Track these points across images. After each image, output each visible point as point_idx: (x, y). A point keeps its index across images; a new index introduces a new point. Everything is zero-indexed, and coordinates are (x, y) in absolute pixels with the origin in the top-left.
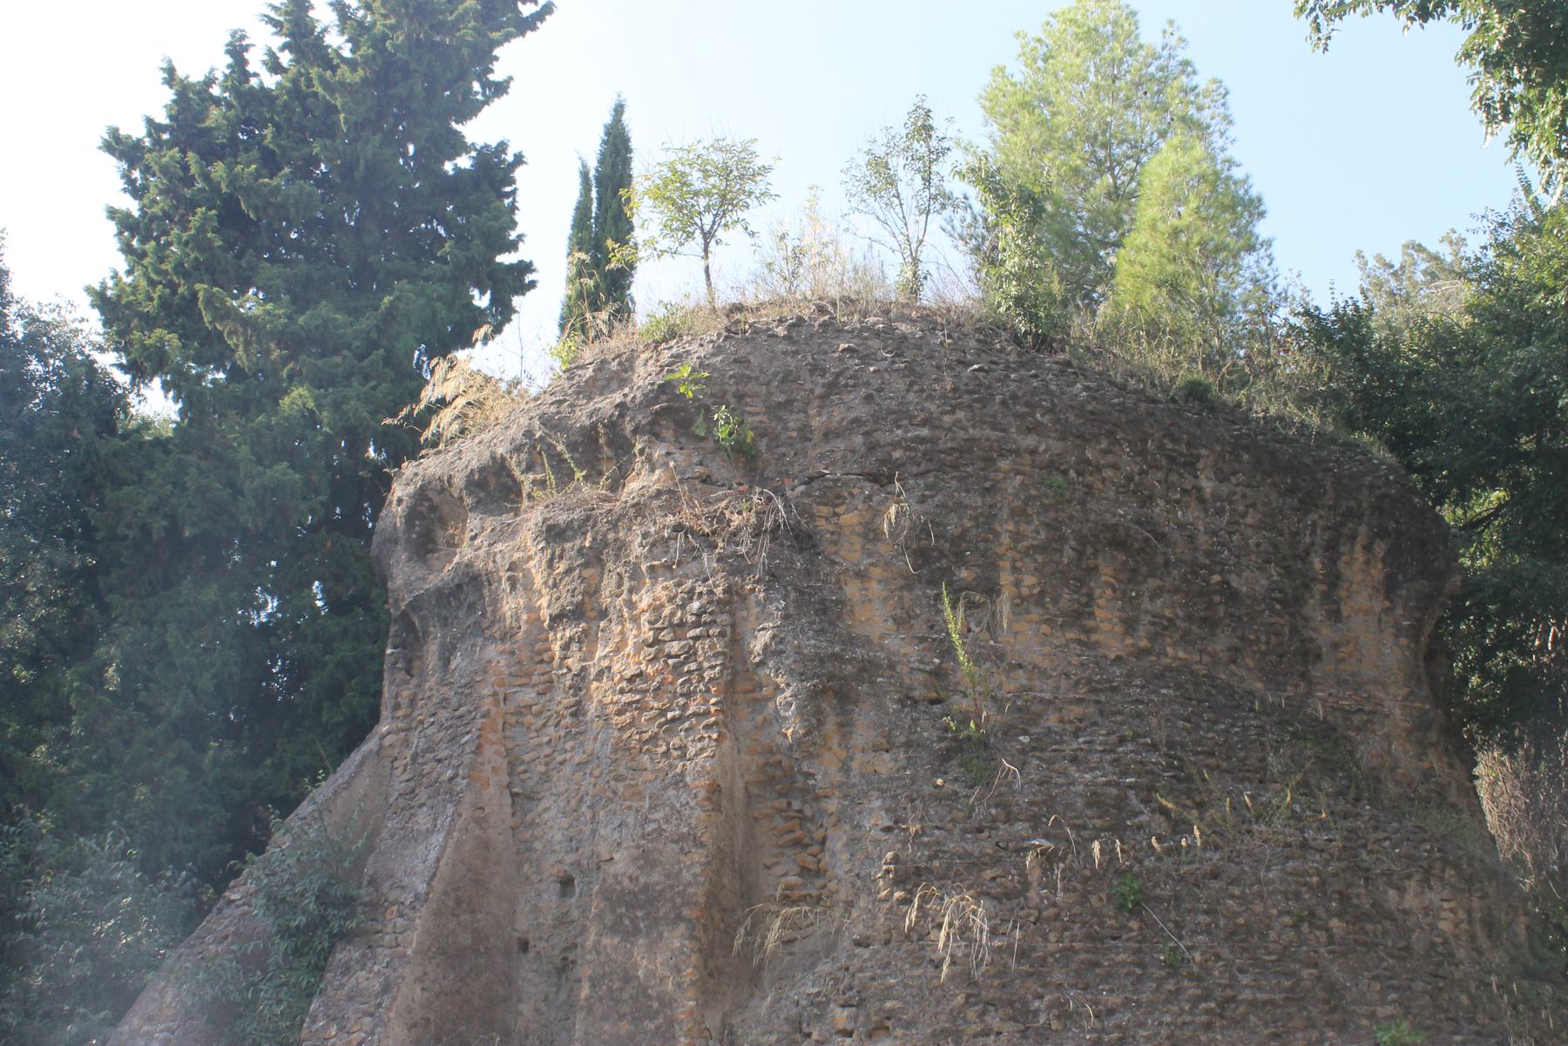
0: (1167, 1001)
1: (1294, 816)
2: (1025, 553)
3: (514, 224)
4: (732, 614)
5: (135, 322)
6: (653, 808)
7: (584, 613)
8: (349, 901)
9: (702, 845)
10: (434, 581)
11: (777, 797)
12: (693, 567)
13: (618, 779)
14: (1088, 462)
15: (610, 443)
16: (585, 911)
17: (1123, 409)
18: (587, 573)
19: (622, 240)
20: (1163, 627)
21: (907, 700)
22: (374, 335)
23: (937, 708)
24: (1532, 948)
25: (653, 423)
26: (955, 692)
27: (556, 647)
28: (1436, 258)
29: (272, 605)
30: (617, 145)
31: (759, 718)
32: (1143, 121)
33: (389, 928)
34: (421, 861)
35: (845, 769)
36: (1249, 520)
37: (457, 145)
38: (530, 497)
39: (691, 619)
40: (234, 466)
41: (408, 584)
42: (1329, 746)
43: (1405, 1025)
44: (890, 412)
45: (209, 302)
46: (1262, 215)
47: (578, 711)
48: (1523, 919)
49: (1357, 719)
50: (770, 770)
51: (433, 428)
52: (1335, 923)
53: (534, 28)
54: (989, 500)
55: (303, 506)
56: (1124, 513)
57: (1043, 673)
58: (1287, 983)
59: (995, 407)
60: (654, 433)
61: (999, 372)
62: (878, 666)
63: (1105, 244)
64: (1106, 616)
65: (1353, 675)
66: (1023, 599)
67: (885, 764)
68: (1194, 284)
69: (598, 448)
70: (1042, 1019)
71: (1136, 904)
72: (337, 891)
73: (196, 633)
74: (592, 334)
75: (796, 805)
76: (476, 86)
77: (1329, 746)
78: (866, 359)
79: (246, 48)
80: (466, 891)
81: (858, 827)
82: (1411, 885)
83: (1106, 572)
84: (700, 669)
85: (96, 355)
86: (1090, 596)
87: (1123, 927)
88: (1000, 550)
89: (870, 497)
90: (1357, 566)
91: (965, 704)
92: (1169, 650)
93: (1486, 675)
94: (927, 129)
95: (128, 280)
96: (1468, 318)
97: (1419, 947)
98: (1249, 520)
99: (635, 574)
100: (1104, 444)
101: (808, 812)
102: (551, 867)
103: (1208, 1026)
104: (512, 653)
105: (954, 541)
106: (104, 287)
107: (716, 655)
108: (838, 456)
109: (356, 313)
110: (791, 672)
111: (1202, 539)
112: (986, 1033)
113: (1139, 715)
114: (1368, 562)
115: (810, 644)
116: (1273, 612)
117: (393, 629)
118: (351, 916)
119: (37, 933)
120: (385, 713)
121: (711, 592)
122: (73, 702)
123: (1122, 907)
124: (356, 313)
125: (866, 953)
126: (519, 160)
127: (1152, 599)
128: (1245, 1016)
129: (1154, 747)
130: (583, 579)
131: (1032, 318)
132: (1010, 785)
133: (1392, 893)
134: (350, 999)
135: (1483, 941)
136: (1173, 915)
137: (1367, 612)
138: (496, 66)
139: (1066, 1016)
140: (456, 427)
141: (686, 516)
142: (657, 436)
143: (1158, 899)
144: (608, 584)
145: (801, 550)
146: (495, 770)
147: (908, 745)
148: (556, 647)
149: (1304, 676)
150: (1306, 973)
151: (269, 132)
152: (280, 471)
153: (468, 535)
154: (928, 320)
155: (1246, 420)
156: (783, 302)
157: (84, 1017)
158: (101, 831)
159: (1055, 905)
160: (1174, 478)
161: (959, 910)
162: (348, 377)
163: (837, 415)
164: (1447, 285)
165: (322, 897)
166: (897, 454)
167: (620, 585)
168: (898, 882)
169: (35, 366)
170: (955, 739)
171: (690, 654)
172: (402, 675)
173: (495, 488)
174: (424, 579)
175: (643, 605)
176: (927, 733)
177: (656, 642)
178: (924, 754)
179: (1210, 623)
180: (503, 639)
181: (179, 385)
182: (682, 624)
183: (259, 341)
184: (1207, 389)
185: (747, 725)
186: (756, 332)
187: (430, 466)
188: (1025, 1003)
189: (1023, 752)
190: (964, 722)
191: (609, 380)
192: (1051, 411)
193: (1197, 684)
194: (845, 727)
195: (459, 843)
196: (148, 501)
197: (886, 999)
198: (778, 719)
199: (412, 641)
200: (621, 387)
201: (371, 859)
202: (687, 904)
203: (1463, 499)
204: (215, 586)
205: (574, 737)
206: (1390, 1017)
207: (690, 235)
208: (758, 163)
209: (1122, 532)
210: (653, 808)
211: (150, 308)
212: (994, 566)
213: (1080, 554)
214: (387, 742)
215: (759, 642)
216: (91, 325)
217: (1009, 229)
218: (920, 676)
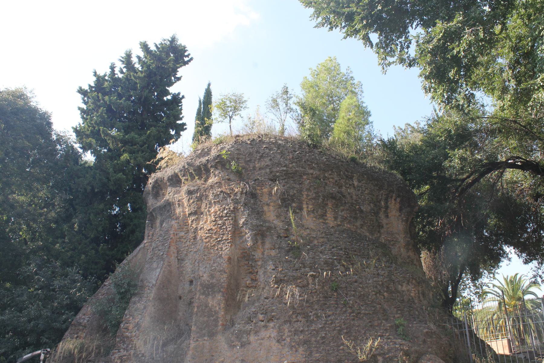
0: (343, 313)
1: (376, 267)
2: (310, 200)
3: (181, 113)
4: (235, 214)
5: (84, 136)
6: (214, 263)
7: (197, 213)
8: (135, 286)
9: (226, 273)
10: (159, 204)
11: (245, 260)
12: (225, 202)
13: (205, 256)
14: (326, 177)
15: (205, 170)
16: (196, 289)
17: (335, 164)
18: (198, 203)
19: (209, 118)
20: (344, 219)
21: (279, 237)
22: (145, 141)
23: (287, 239)
24: (434, 301)
25: (215, 165)
26: (291, 235)
27: (190, 222)
28: (413, 127)
29: (117, 209)
30: (208, 94)
31: (241, 241)
32: (341, 91)
33: (146, 292)
34: (153, 276)
35: (263, 254)
36: (366, 192)
37: (167, 93)
38: (184, 183)
39: (224, 215)
40: (108, 173)
41: (152, 205)
42: (384, 249)
43: (402, 319)
44: (276, 163)
45: (103, 132)
46: (370, 115)
47: (195, 238)
48: (431, 293)
49: (392, 243)
50: (244, 254)
51: (159, 165)
52: (385, 294)
53: (188, 64)
54: (301, 186)
55: (126, 184)
56: (335, 190)
57: (314, 230)
58: (373, 309)
59: (303, 163)
60: (216, 167)
61: (304, 154)
62: (272, 228)
63: (331, 122)
64: (330, 216)
65: (391, 232)
66: (309, 211)
67: (273, 253)
68: (353, 132)
69: (202, 171)
70: (312, 318)
71: (336, 289)
72: (133, 283)
73: (98, 216)
74: (201, 142)
75: (250, 263)
76: (173, 78)
77: (384, 249)
78: (270, 150)
79: (115, 67)
80: (166, 283)
81: (266, 269)
82: (405, 284)
83: (330, 205)
84: (226, 228)
85: (74, 144)
86: (326, 211)
87: (333, 295)
88: (303, 199)
89: (270, 185)
90: (393, 204)
91: (294, 238)
92: (346, 225)
93: (423, 232)
94: (287, 92)
95: (83, 125)
96: (421, 143)
97: (406, 300)
98: (366, 192)
99: (210, 203)
100: (330, 173)
101: (253, 265)
102: (187, 278)
103: (353, 320)
104: (178, 223)
105: (292, 196)
106: (77, 127)
107: (231, 224)
108: (263, 174)
109: (140, 135)
110: (250, 229)
111: (354, 197)
112: (297, 321)
113: (338, 241)
114: (395, 203)
115: (255, 222)
116: (372, 216)
117: (148, 216)
118: (136, 289)
119: (56, 292)
120: (146, 237)
121: (229, 208)
122: (66, 234)
123: (332, 290)
124: (140, 135)
125: (268, 301)
126: (183, 97)
127: (341, 212)
128: (362, 317)
129: (341, 249)
130: (197, 204)
131: (313, 140)
132: (305, 258)
133: (400, 286)
134: (136, 310)
135: (422, 298)
136: (345, 292)
137: (395, 216)
138: (178, 73)
139: (318, 317)
140: (165, 165)
141: (223, 189)
142: (217, 168)
143: (342, 288)
144: (203, 206)
145: (253, 198)
146: (173, 253)
147: (279, 248)
148: (190, 222)
149: (379, 232)
150: (378, 306)
151: (120, 89)
152: (120, 175)
153: (168, 192)
154: (286, 140)
155: (366, 167)
156: (249, 135)
157: (67, 314)
158: (72, 266)
159: (315, 289)
160: (347, 181)
161: (291, 291)
162: (138, 151)
163: (263, 164)
164: (416, 134)
165: (129, 284)
166: (278, 174)
167: (206, 206)
168: (276, 283)
169: (58, 147)
170: (291, 247)
171: (224, 224)
172: (150, 228)
173: (175, 180)
174: (156, 204)
175: (212, 211)
176: (284, 245)
177: (215, 221)
178: (283, 250)
179: (356, 218)
180: (176, 219)
181: (95, 153)
182: (222, 216)
183: (116, 142)
184: (356, 159)
185: (238, 242)
186: (242, 142)
187: (158, 175)
188: (308, 314)
189: (308, 250)
190: (293, 242)
191: (205, 154)
192: (317, 164)
193: (352, 234)
194: (263, 243)
195: (164, 271)
196: (86, 182)
197: (273, 312)
198: (246, 241)
199: (153, 220)
200: (208, 156)
201: (141, 275)
202: (222, 288)
203: (419, 188)
204: (103, 204)
205: (194, 245)
206: (398, 317)
207: (226, 117)
208: (244, 99)
209: (334, 195)
210: (214, 263)
211: (88, 133)
212: (302, 203)
213: (324, 200)
214: (146, 245)
215: (242, 221)
216: (73, 137)
217: (307, 118)
218: (283, 231)
